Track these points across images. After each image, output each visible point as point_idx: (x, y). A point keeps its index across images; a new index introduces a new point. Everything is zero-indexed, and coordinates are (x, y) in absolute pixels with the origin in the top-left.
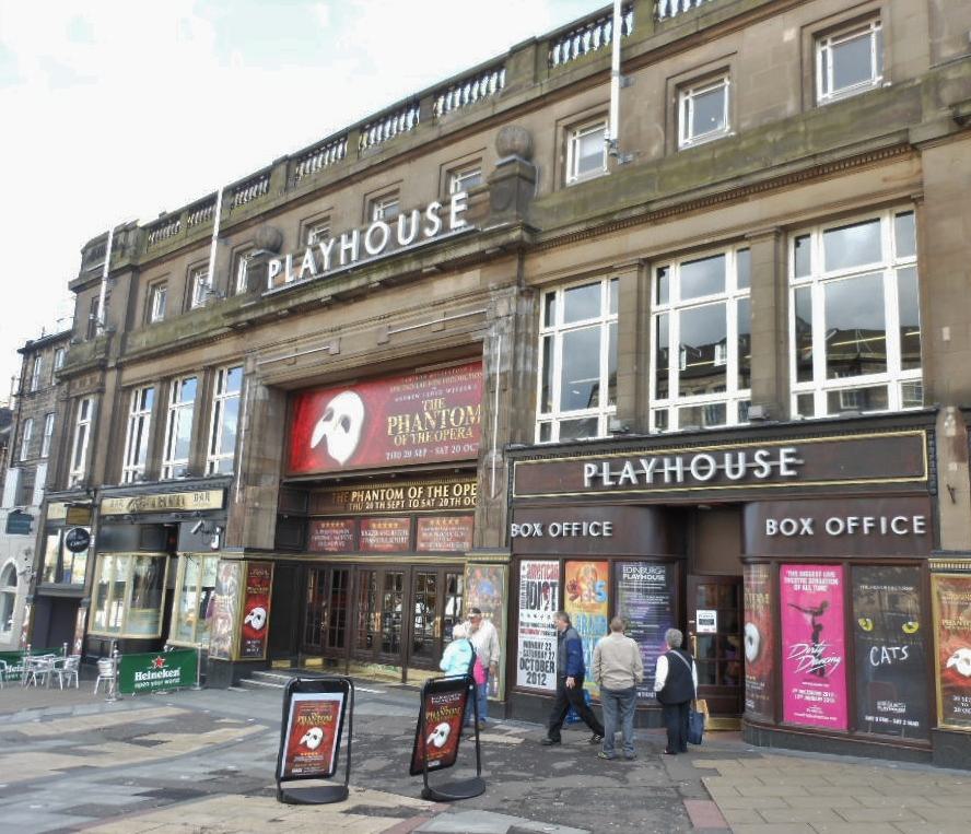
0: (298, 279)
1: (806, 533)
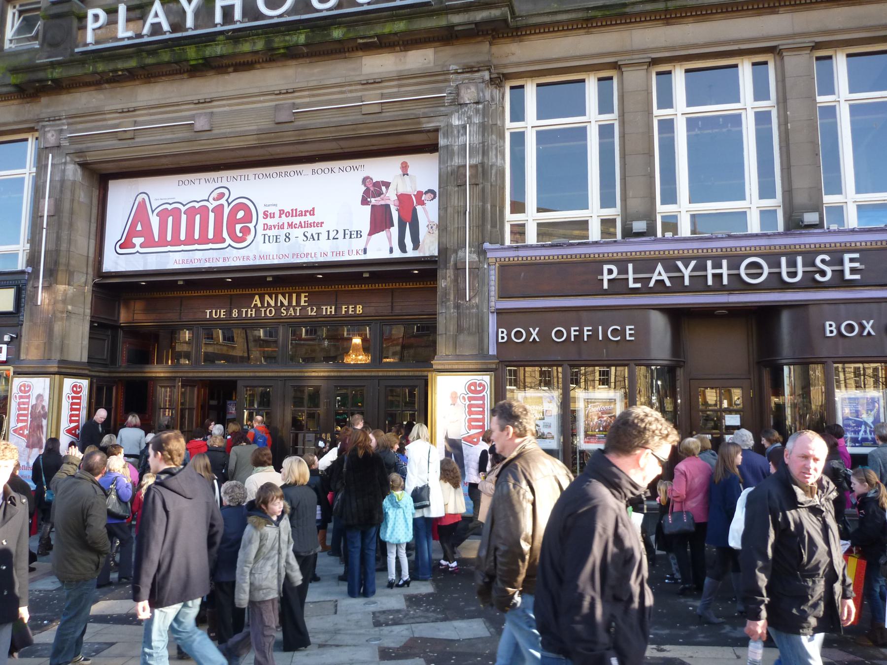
0: (139, 36)
1: (869, 333)
